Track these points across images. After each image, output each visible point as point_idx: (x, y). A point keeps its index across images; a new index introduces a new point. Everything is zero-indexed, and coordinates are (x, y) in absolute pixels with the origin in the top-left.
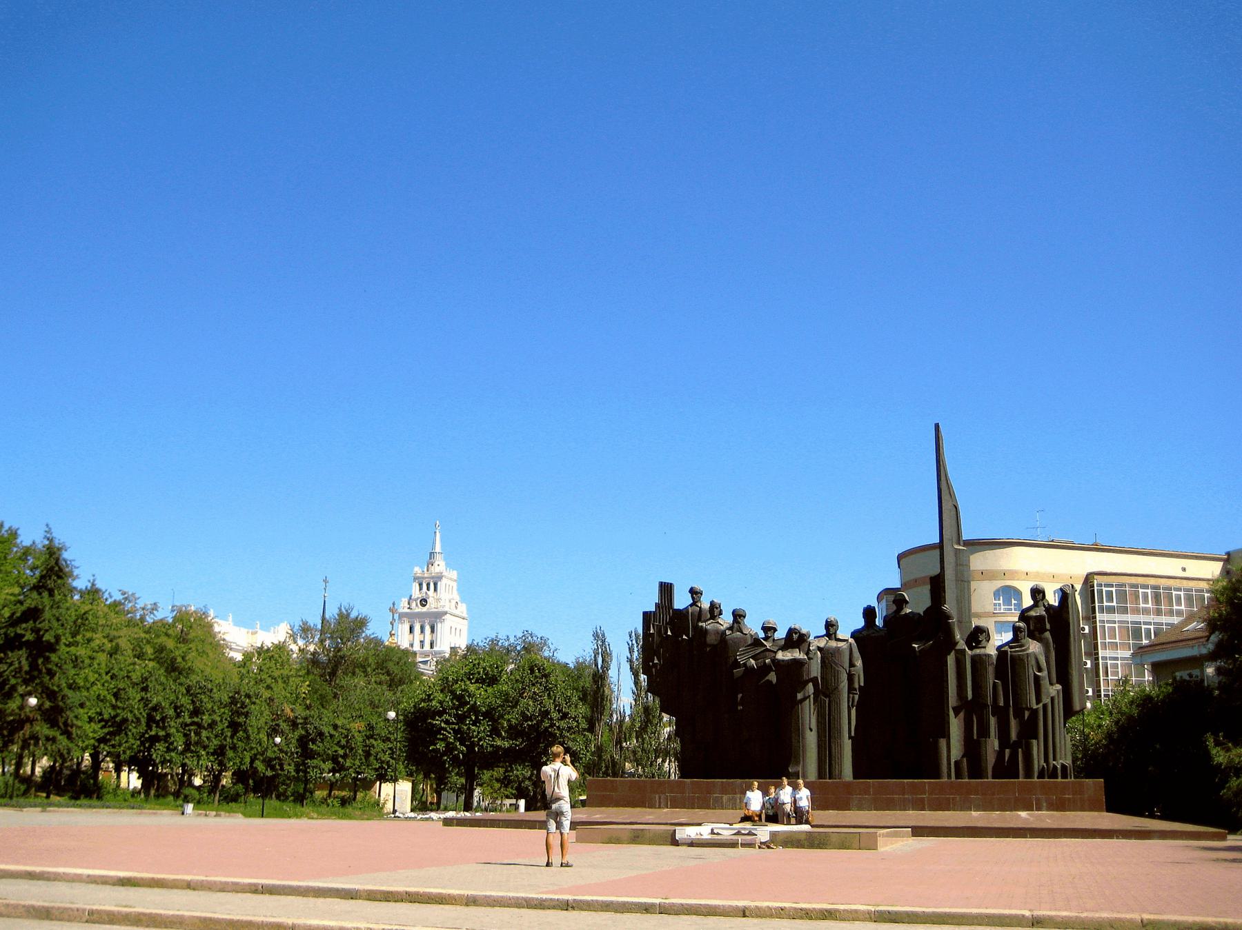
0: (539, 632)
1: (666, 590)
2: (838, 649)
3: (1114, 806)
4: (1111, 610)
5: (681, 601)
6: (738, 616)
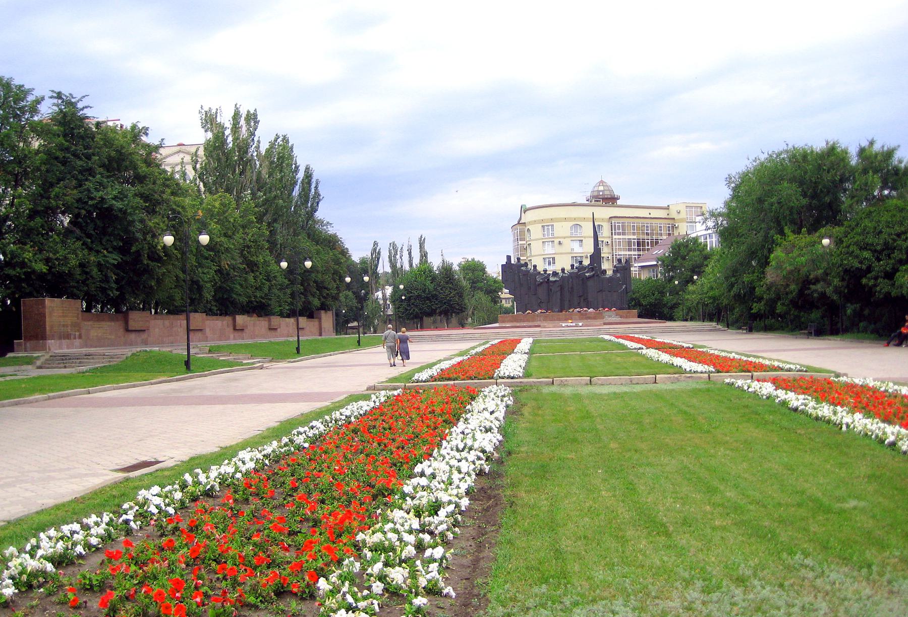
1: (509, 258)
3: (640, 316)
4: (619, 234)
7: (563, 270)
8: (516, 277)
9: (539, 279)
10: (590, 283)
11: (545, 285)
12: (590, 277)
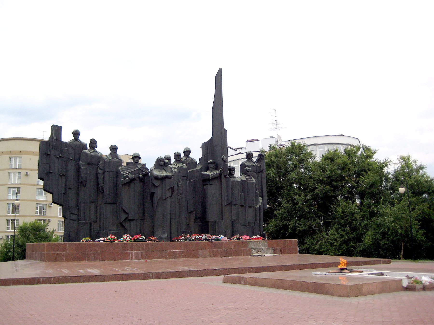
11: (137, 186)
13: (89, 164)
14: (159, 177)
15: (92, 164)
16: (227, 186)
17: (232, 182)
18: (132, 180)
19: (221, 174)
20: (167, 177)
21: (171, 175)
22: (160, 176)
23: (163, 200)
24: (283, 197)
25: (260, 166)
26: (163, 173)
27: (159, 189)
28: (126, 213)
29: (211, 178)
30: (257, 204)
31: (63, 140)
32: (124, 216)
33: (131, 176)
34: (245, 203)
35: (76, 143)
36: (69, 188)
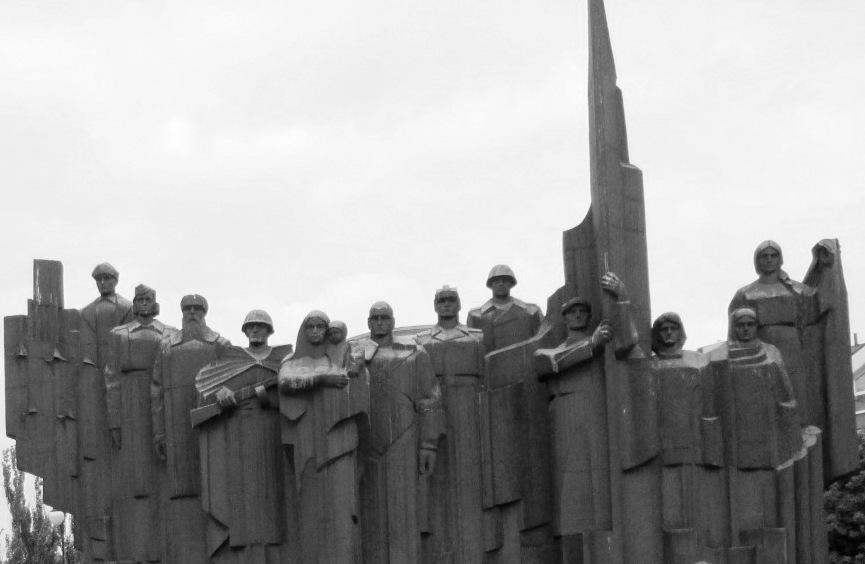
0: (446, 284)
1: (49, 274)
2: (397, 362)
5: (79, 294)
6: (194, 309)
7: (381, 321)
8: (88, 379)
9: (213, 386)
10: (575, 406)
11: (252, 428)
12: (572, 368)
13: (125, 372)
14: (294, 386)
15: (135, 370)
16: (637, 394)
17: (664, 372)
18: (228, 411)
19: (599, 351)
20: (321, 385)
21: (344, 372)
22: (298, 381)
23: (320, 470)
24: (108, 375)
25: (816, 297)
26: (322, 368)
27: (304, 430)
28: (220, 524)
29: (556, 369)
30: (787, 450)
31: (68, 305)
32: (217, 539)
33: (226, 393)
34: (726, 452)
35: (106, 306)
36: (85, 458)
